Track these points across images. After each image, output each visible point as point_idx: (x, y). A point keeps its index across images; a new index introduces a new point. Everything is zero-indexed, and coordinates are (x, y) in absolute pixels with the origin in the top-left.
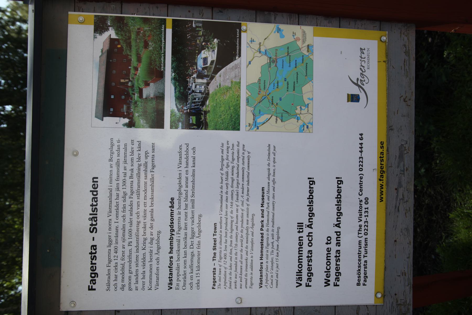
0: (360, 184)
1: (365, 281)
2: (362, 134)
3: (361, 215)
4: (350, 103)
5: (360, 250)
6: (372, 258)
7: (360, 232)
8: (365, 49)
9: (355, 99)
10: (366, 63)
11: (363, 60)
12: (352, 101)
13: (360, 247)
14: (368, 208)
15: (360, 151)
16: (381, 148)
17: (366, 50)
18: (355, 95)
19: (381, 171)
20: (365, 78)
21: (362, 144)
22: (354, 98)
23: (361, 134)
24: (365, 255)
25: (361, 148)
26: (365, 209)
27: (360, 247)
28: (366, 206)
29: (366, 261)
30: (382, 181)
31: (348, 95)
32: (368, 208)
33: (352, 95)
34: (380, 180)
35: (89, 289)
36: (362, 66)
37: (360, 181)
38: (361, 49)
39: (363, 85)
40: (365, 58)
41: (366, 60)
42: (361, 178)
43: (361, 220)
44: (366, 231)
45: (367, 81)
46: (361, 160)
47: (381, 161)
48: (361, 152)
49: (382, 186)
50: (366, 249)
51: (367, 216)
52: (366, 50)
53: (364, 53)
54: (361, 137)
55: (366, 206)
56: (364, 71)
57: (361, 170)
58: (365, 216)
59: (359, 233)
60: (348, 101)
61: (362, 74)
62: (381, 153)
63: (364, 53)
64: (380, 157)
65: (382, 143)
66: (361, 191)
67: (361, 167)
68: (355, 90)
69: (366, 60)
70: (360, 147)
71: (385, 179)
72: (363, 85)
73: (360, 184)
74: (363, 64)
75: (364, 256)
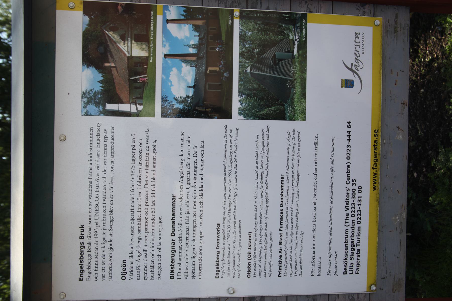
0: (347, 172)
1: (358, 269)
2: (350, 122)
3: (348, 204)
4: (344, 88)
5: (347, 239)
6: (364, 246)
7: (347, 221)
8: (359, 34)
9: (349, 84)
10: (361, 48)
11: (357, 44)
12: (346, 87)
13: (347, 236)
14: (361, 197)
15: (348, 140)
16: (375, 136)
17: (361, 34)
18: (349, 80)
19: (374, 159)
20: (360, 63)
21: (350, 132)
22: (348, 84)
23: (349, 122)
24: (358, 244)
25: (349, 136)
26: (359, 197)
27: (347, 236)
28: (360, 195)
29: (358, 250)
30: (375, 170)
31: (342, 80)
32: (361, 197)
33: (346, 80)
34: (374, 169)
35: (79, 280)
36: (356, 51)
37: (348, 170)
38: (356, 33)
39: (358, 70)
40: (359, 43)
41: (360, 44)
42: (349, 167)
43: (348, 209)
44: (359, 220)
45: (361, 66)
46: (349, 148)
47: (375, 150)
48: (349, 140)
49: (375, 175)
50: (359, 237)
51: (361, 205)
52: (361, 34)
53: (358, 38)
54: (348, 125)
55: (360, 195)
56: (358, 56)
57: (348, 158)
58: (358, 205)
59: (345, 222)
60: (342, 87)
61: (357, 59)
62: (375, 141)
63: (358, 38)
64: (374, 146)
65: (376, 131)
66: (348, 180)
67: (348, 155)
68: (349, 76)
69: (360, 44)
70: (348, 136)
71: (379, 166)
72: (358, 70)
73: (347, 172)
74: (358, 48)
75: (357, 245)
